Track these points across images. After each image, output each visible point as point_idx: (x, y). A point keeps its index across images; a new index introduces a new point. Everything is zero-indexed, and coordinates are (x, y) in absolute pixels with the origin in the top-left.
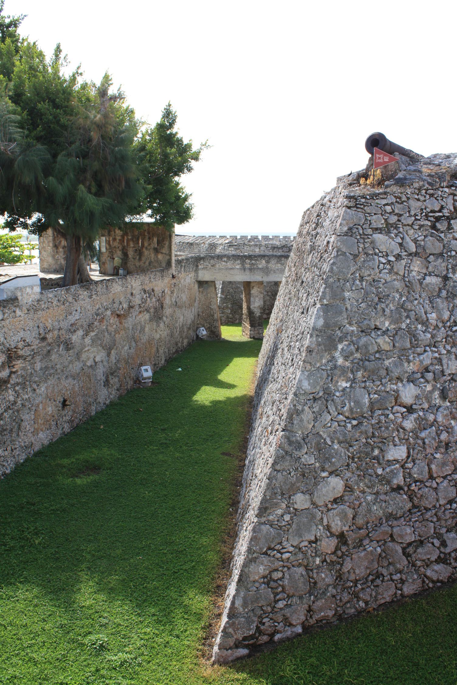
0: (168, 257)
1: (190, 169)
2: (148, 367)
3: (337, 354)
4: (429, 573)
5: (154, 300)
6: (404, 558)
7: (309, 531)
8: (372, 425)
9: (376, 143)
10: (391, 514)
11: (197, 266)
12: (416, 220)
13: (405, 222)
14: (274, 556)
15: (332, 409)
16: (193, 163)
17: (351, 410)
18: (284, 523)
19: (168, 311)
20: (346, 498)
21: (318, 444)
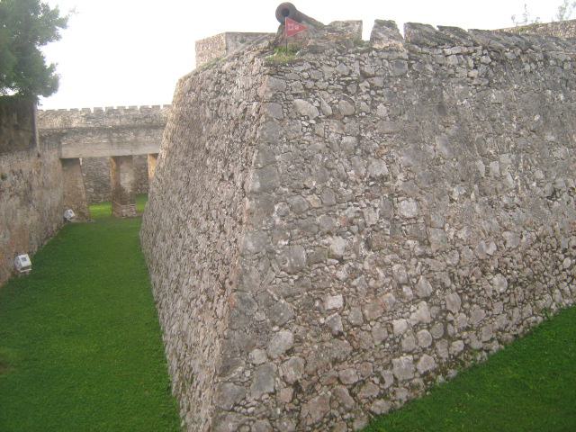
0: (31, 134)
1: (58, 38)
2: (26, 256)
3: (274, 215)
4: (372, 408)
5: (23, 182)
6: (351, 398)
7: (269, 384)
8: (312, 278)
9: (286, 13)
10: (336, 359)
11: (60, 143)
12: (330, 84)
13: (321, 87)
14: (240, 412)
15: (275, 266)
16: (60, 31)
17: (292, 267)
18: (245, 379)
19: (36, 193)
20: (296, 349)
21: (267, 300)
